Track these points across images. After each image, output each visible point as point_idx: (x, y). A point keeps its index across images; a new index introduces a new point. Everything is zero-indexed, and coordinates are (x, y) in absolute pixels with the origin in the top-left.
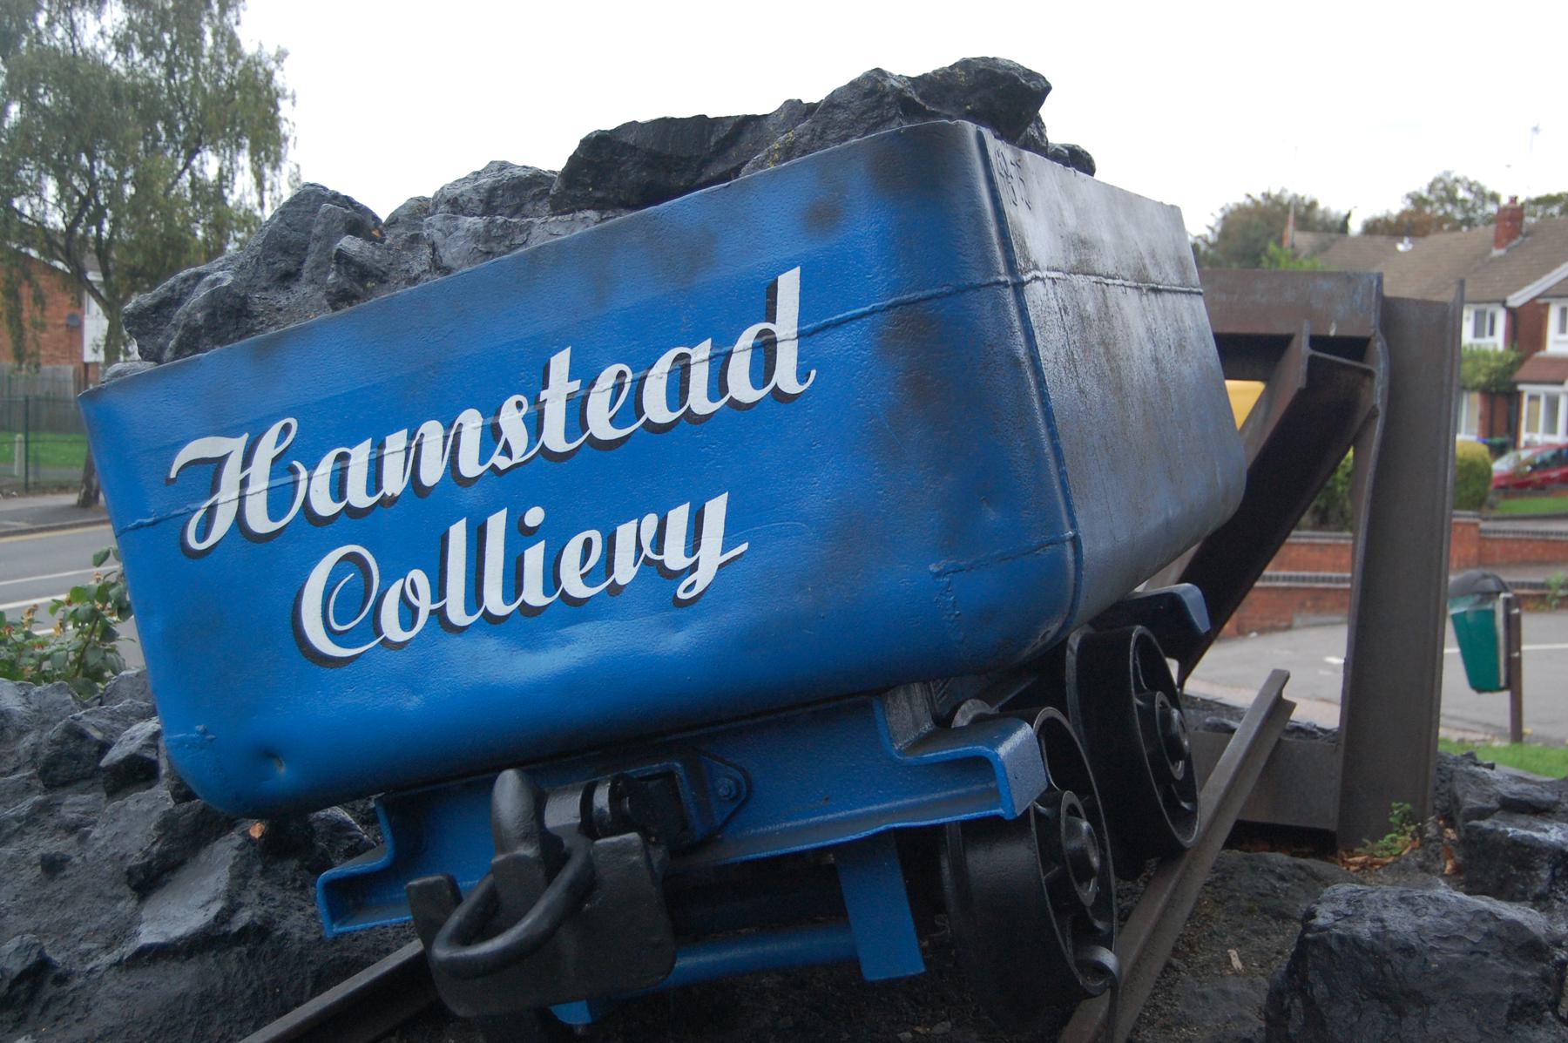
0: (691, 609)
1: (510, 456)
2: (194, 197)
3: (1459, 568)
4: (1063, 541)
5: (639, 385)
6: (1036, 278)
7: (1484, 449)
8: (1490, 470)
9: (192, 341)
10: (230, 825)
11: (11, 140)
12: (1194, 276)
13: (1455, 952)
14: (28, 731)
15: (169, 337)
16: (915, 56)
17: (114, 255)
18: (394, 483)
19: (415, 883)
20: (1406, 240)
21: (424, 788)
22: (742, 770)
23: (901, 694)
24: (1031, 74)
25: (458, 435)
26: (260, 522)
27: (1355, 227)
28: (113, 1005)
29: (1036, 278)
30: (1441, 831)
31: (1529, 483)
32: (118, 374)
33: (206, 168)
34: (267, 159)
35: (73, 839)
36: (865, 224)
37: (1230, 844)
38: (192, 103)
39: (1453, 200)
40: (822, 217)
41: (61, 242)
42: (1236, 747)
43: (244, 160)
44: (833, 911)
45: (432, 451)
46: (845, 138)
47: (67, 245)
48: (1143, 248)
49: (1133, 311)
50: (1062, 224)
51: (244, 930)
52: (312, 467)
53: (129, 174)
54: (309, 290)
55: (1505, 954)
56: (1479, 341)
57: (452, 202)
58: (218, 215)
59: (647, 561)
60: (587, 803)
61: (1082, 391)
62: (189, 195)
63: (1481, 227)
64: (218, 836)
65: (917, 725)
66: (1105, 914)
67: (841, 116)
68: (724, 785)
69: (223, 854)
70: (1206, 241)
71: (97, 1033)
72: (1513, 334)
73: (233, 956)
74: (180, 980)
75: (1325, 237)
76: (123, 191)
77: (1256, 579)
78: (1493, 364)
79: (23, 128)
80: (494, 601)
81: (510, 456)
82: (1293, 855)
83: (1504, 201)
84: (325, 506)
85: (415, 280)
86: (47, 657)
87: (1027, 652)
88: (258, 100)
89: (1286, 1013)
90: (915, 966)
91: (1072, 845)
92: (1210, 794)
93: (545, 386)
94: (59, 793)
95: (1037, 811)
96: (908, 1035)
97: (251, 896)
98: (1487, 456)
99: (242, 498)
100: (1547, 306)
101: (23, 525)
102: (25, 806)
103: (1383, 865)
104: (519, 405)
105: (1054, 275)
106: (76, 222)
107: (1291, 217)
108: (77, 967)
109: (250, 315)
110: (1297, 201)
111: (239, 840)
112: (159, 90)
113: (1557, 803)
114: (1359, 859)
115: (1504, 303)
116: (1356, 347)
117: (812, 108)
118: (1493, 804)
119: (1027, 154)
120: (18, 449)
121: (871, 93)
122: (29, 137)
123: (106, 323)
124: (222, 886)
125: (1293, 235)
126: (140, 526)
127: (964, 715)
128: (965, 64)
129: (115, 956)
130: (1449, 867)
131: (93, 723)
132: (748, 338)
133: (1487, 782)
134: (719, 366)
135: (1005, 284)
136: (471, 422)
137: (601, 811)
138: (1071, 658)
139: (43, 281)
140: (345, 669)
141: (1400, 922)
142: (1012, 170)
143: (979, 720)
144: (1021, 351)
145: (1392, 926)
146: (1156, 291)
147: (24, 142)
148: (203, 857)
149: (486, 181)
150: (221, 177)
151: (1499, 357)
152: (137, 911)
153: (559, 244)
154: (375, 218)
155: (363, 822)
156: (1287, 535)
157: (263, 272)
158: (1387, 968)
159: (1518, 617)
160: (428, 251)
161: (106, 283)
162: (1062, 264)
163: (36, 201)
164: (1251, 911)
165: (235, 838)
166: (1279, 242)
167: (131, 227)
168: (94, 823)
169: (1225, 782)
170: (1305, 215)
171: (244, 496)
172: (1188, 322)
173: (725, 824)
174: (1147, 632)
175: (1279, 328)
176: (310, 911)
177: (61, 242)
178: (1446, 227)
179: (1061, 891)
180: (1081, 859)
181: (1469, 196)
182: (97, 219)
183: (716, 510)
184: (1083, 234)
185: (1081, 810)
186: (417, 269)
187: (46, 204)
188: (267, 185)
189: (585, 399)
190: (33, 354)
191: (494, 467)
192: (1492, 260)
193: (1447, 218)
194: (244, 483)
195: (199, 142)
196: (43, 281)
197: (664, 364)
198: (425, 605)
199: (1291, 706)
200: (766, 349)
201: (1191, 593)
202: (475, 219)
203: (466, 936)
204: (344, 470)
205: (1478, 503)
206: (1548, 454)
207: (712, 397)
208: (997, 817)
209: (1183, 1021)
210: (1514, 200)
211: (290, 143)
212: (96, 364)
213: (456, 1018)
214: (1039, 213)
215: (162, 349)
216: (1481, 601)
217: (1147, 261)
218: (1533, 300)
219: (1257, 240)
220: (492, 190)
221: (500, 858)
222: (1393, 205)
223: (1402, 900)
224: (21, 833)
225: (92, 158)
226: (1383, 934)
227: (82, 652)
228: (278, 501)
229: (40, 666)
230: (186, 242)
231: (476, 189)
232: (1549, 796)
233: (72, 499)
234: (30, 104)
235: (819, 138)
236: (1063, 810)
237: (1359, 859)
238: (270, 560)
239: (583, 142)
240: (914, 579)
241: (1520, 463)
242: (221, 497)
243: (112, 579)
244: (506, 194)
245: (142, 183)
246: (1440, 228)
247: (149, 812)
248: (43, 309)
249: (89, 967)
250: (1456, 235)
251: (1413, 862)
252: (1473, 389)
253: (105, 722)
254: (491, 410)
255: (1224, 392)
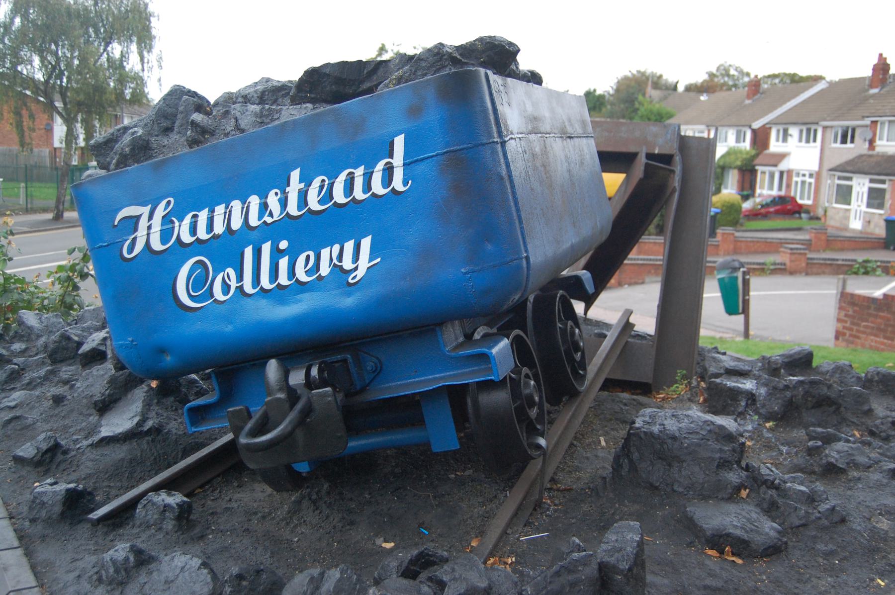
0: (356, 286)
1: (272, 217)
2: (109, 66)
3: (724, 255)
4: (521, 259)
5: (331, 186)
6: (512, 138)
7: (739, 197)
8: (741, 207)
9: (124, 161)
10: (142, 381)
11: (16, 36)
12: (590, 128)
13: (695, 439)
14: (42, 336)
15: (113, 158)
16: (457, 36)
17: (69, 94)
18: (219, 228)
19: (230, 409)
20: (705, 95)
21: (234, 366)
22: (377, 358)
23: (449, 326)
24: (511, 44)
25: (248, 207)
26: (157, 245)
27: (681, 88)
28: (89, 464)
29: (512, 138)
30: (699, 383)
31: (759, 214)
32: (90, 176)
33: (114, 51)
34: (145, 47)
35: (67, 387)
36: (434, 115)
37: (604, 387)
38: (107, 19)
39: (728, 75)
40: (414, 111)
41: (42, 88)
42: (607, 344)
43: (134, 47)
44: (419, 421)
45: (236, 214)
46: (425, 75)
47: (45, 89)
48: (564, 118)
49: (558, 147)
50: (525, 111)
51: (150, 430)
52: (181, 220)
53: (76, 54)
54: (178, 137)
55: (717, 440)
56: (738, 145)
57: (244, 98)
58: (121, 75)
59: (335, 265)
60: (308, 374)
61: (532, 189)
62: (106, 65)
63: (741, 89)
64: (136, 386)
65: (457, 339)
66: (542, 423)
67: (423, 64)
68: (370, 366)
69: (139, 394)
70: (609, 93)
71: (83, 477)
72: (754, 142)
73: (145, 442)
74: (120, 452)
75: (666, 93)
76: (73, 63)
77: (624, 259)
78: (744, 156)
79: (23, 31)
80: (265, 283)
81: (272, 217)
82: (633, 394)
83: (752, 76)
84: (187, 238)
85: (227, 135)
86: (45, 298)
87: (505, 307)
88: (140, 17)
89: (621, 466)
90: (454, 445)
91: (527, 391)
92: (592, 368)
93: (288, 185)
94: (58, 366)
95: (510, 377)
96: (453, 476)
97: (152, 414)
98: (740, 201)
99: (148, 234)
100: (770, 128)
101: (26, 229)
102: (42, 372)
103: (673, 399)
104: (276, 194)
105: (520, 136)
106: (50, 77)
107: (650, 83)
108: (72, 447)
109: (150, 149)
110: (653, 75)
111: (146, 389)
112: (91, 12)
113: (750, 371)
114: (661, 396)
115: (750, 127)
116: (667, 159)
117: (411, 58)
118: (722, 371)
119: (509, 79)
120: (22, 191)
121: (438, 54)
122: (25, 35)
123: (65, 128)
124: (139, 410)
125: (651, 92)
126: (102, 246)
127: (479, 333)
128: (481, 39)
129: (90, 441)
130: (702, 399)
131: (74, 333)
132: (381, 165)
133: (720, 361)
134: (368, 177)
135: (497, 143)
136: (254, 201)
137: (314, 377)
138: (530, 306)
139: (33, 106)
140: (197, 313)
141: (672, 425)
142: (502, 88)
143: (485, 336)
144: (504, 172)
145: (668, 427)
146: (570, 138)
147: (23, 38)
148: (129, 396)
149: (260, 88)
150: (122, 55)
151: (747, 153)
152: (99, 421)
153: (294, 121)
154: (208, 102)
155: (202, 379)
156: (640, 237)
157: (156, 127)
158: (665, 446)
159: (749, 280)
160: (233, 120)
161: (65, 108)
162: (525, 130)
163: (29, 67)
164: (611, 420)
165: (144, 387)
166: (644, 95)
167: (77, 82)
168: (77, 380)
169: (600, 361)
170: (657, 82)
171: (150, 233)
172: (586, 151)
173: (371, 382)
174: (565, 293)
175: (632, 149)
176: (180, 420)
177: (42, 88)
178: (724, 88)
179: (521, 413)
180: (530, 398)
181: (736, 73)
182: (60, 76)
183: (366, 243)
184: (536, 114)
185: (531, 375)
186: (229, 129)
187: (34, 69)
188: (146, 60)
189: (307, 191)
190: (29, 144)
191: (265, 222)
192: (745, 106)
193: (725, 84)
194: (149, 228)
195: (111, 38)
196: (33, 106)
197: (343, 176)
198: (233, 284)
199: (633, 325)
200: (389, 171)
201: (586, 275)
202: (255, 106)
203: (255, 433)
204: (196, 222)
205: (735, 223)
206: (769, 200)
207: (364, 192)
208: (491, 380)
209: (578, 469)
210: (756, 76)
211: (157, 38)
212: (60, 148)
213: (249, 469)
214: (513, 105)
215: (109, 163)
216: (732, 272)
217: (566, 124)
218: (764, 125)
219: (633, 94)
220: (263, 93)
221: (269, 398)
222: (700, 77)
223: (673, 416)
224: (41, 384)
225: (57, 46)
226: (664, 430)
227: (63, 296)
228: (165, 235)
229: (43, 302)
230: (105, 88)
231: (256, 92)
232: (747, 368)
233: (50, 216)
234: (25, 17)
235: (413, 75)
236: (522, 376)
237: (661, 396)
238: (161, 263)
239: (306, 72)
240: (454, 275)
241: (756, 204)
242: (138, 234)
243: (77, 262)
244: (271, 94)
245: (83, 59)
246: (721, 89)
247: (103, 375)
248: (33, 122)
249: (78, 446)
250: (729, 93)
251: (685, 397)
252: (735, 168)
253: (79, 332)
254: (264, 196)
255: (601, 180)
